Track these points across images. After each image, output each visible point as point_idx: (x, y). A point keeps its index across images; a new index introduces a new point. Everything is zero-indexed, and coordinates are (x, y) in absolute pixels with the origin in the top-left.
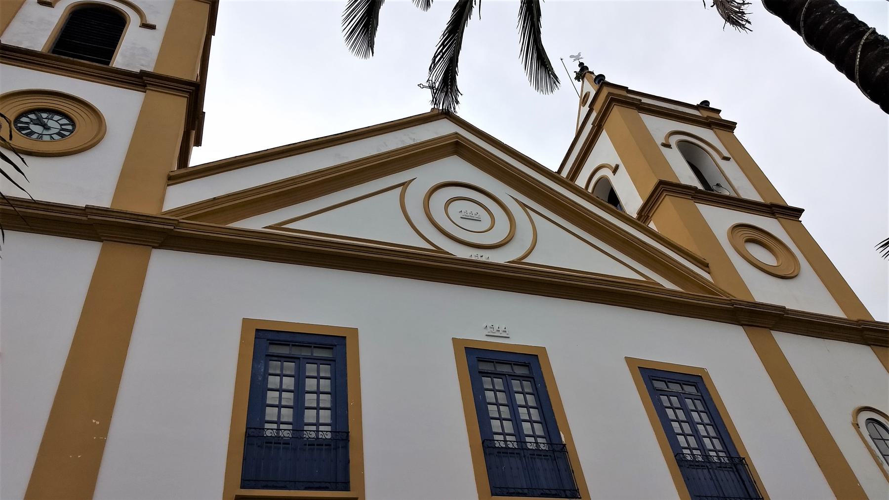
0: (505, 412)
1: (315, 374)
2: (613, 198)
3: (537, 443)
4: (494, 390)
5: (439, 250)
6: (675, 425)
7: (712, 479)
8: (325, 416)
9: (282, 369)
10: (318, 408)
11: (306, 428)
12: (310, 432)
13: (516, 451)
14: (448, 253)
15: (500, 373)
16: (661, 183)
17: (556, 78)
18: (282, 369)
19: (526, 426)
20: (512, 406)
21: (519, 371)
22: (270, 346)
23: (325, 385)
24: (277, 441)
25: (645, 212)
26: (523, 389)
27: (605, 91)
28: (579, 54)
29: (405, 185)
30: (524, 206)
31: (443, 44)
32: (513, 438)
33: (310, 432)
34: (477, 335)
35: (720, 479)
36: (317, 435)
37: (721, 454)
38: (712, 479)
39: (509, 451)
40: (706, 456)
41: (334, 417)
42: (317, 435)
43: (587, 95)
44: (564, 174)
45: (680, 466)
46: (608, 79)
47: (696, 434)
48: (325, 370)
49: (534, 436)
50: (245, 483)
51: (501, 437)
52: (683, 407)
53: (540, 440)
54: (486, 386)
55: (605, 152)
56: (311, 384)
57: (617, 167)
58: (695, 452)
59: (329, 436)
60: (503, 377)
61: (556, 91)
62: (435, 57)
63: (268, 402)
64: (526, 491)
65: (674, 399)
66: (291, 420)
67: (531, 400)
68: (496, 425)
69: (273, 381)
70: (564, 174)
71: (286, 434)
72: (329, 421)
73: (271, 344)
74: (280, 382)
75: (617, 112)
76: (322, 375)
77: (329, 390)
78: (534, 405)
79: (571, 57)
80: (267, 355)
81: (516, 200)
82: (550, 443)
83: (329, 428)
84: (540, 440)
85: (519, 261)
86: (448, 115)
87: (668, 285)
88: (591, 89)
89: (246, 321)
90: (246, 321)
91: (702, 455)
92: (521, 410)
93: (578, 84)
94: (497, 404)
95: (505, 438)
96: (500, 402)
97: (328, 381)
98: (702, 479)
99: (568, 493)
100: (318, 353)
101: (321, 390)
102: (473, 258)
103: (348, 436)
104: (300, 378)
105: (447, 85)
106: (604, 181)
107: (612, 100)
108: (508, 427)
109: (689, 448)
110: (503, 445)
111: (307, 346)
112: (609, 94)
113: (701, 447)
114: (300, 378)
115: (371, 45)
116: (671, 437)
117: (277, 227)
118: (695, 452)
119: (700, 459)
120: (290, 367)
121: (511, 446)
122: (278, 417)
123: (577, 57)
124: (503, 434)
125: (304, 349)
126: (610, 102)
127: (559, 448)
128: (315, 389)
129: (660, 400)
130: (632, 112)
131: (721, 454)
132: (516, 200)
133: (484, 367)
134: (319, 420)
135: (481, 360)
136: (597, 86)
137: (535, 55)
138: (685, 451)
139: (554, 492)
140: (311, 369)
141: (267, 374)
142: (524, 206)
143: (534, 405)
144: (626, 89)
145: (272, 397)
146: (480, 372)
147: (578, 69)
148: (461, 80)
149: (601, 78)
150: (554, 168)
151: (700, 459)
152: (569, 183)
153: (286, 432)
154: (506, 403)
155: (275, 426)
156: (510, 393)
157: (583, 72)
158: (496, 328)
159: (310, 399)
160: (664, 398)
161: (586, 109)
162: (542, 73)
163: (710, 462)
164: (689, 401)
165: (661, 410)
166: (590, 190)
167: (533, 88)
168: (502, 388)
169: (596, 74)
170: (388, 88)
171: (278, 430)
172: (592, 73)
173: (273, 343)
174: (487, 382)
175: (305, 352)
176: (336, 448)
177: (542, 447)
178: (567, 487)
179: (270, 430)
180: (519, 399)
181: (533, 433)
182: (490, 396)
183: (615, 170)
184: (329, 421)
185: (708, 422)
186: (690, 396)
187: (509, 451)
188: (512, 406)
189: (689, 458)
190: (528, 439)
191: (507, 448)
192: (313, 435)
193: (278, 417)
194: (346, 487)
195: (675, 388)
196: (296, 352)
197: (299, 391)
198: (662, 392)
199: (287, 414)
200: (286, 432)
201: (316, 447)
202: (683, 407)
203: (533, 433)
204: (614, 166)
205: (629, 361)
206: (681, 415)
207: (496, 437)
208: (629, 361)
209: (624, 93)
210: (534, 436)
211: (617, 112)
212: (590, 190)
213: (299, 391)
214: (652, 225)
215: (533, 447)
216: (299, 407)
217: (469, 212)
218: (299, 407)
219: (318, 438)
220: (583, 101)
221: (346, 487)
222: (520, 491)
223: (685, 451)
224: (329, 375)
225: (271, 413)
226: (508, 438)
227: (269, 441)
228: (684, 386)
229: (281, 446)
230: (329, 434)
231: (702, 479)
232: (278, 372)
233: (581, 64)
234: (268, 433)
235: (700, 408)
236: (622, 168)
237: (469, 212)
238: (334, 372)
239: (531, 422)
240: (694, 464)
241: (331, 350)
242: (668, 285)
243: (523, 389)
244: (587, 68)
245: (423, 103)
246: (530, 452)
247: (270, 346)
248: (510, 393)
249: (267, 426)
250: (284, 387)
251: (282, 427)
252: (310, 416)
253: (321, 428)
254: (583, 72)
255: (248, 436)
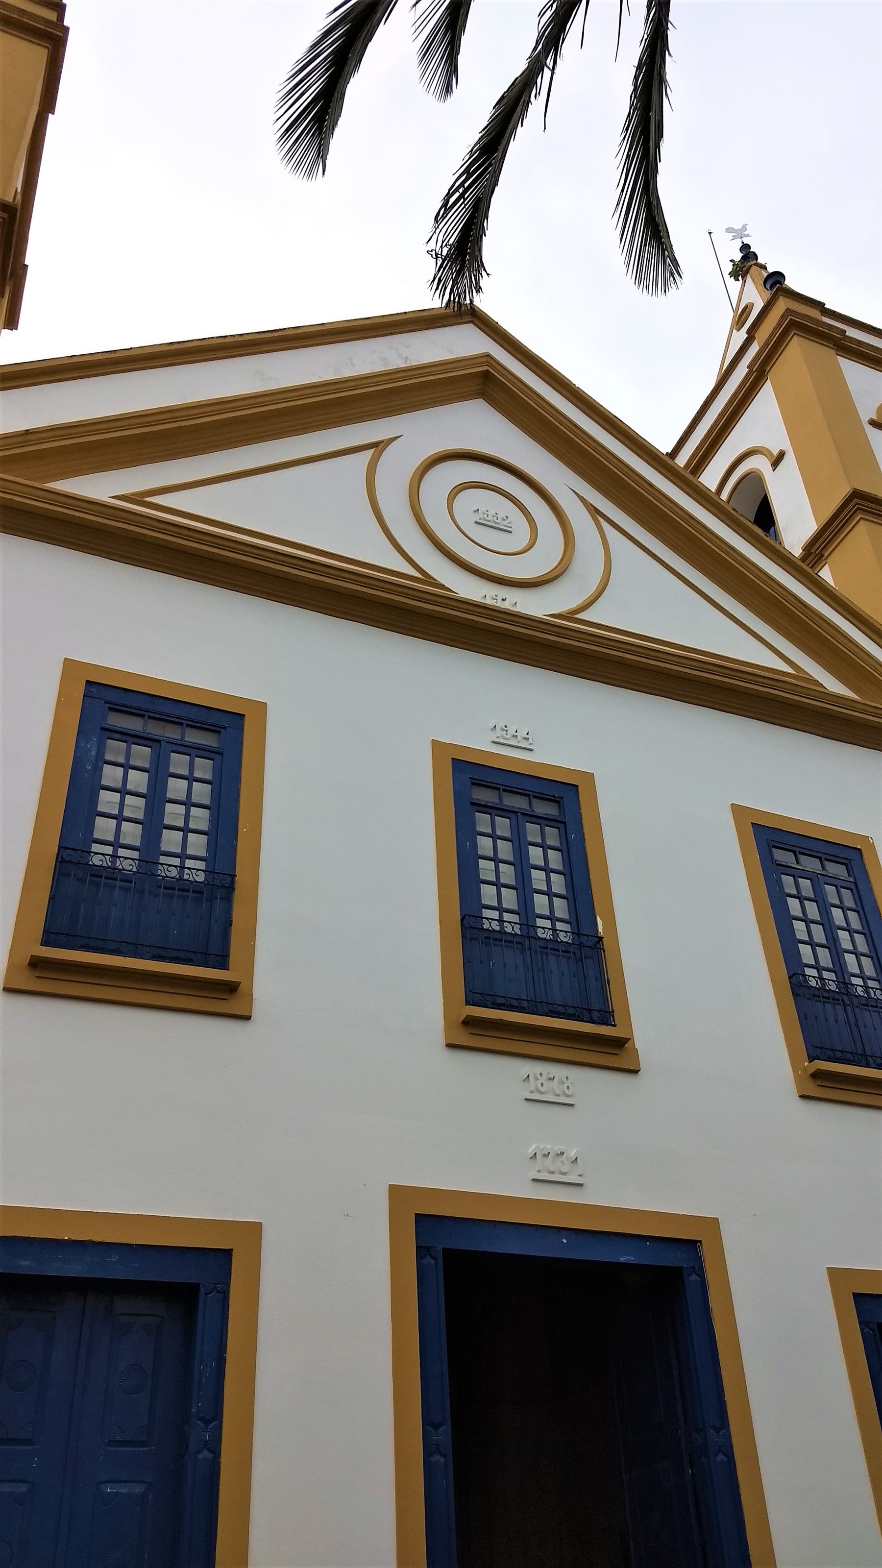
0: (508, 873)
1: (186, 772)
2: (765, 517)
3: (554, 930)
4: (494, 836)
5: (428, 579)
6: (799, 926)
7: (848, 1023)
8: (197, 844)
9: (128, 755)
10: (186, 830)
11: (163, 859)
12: (168, 867)
13: (515, 940)
14: (442, 587)
15: (508, 808)
16: (856, 495)
17: (676, 264)
18: (128, 755)
19: (540, 902)
20: (522, 866)
21: (542, 808)
22: (111, 713)
23: (202, 792)
24: (110, 875)
25: (819, 547)
26: (543, 839)
27: (782, 305)
28: (744, 227)
29: (378, 447)
30: (595, 512)
31: (467, 171)
32: (515, 918)
33: (168, 867)
34: (477, 740)
35: (861, 1025)
36: (181, 873)
37: (871, 984)
38: (848, 1023)
39: (505, 938)
40: (844, 983)
41: (212, 846)
42: (181, 873)
43: (748, 309)
44: (681, 461)
45: (795, 994)
46: (791, 282)
47: (833, 945)
48: (204, 768)
49: (552, 918)
50: (49, 938)
51: (495, 915)
52: (819, 899)
53: (559, 926)
54: (480, 828)
55: (764, 423)
56: (176, 788)
57: (781, 455)
58: (826, 975)
59: (201, 877)
60: (511, 815)
61: (672, 291)
62: (449, 195)
63: (101, 808)
64: (525, 1004)
65: (805, 884)
66: (137, 843)
67: (555, 859)
68: (488, 893)
69: (111, 775)
70: (681, 461)
71: (126, 865)
72: (203, 853)
73: (111, 709)
74: (123, 779)
75: (797, 349)
76: (197, 774)
77: (207, 802)
78: (560, 867)
79: (729, 230)
80: (103, 729)
81: (582, 499)
82: (577, 933)
83: (201, 865)
84: (559, 926)
85: (570, 616)
86: (462, 313)
87: (833, 685)
88: (756, 298)
89: (69, 665)
90: (69, 665)
91: (837, 982)
92: (535, 873)
93: (735, 286)
94: (496, 860)
95: (501, 916)
96: (501, 856)
97: (208, 787)
98: (832, 1020)
99: (595, 1015)
100: (194, 737)
101: (194, 799)
102: (488, 601)
103: (233, 882)
104: (158, 775)
105: (463, 256)
106: (754, 480)
107: (793, 325)
108: (510, 898)
109: (862, 976)
110: (496, 926)
111: (176, 721)
112: (788, 311)
113: (839, 967)
114: (158, 775)
115: (322, 153)
116: (788, 944)
117: (137, 498)
118: (826, 975)
119: (833, 987)
120: (142, 754)
121: (509, 929)
122: (115, 835)
123: (739, 233)
124: (500, 909)
125: (170, 727)
126: (787, 326)
127: (591, 942)
128: (183, 797)
129: (780, 883)
130: (825, 353)
131: (871, 984)
132: (582, 499)
133: (784, 857)
134: (185, 848)
135: (476, 783)
136: (768, 295)
137: (643, 215)
138: (855, 981)
139: (571, 1011)
140: (178, 762)
141: (101, 761)
142: (595, 512)
143: (560, 867)
144: (819, 305)
145: (108, 801)
146: (472, 804)
147: (738, 256)
148: (491, 247)
149: (775, 280)
150: (665, 446)
151: (833, 987)
152: (687, 480)
153: (128, 860)
154: (511, 859)
155: (109, 850)
156: (519, 843)
157: (746, 263)
158: (511, 731)
159: (173, 813)
160: (787, 880)
161: (741, 336)
162: (650, 252)
163: (848, 994)
164: (830, 890)
165: (777, 900)
166: (724, 496)
167: (630, 279)
168: (557, 844)
169: (771, 270)
170: (349, 248)
171: (115, 856)
172: (764, 267)
173: (116, 708)
174: (483, 821)
175: (172, 733)
176: (212, 899)
177: (562, 937)
178: (595, 1005)
179: (99, 856)
180: (535, 855)
181: (551, 912)
182: (485, 845)
183: (777, 461)
184: (203, 853)
185: (860, 928)
186: (833, 881)
187: (505, 938)
188: (522, 866)
189: (813, 983)
190: (540, 922)
191: (502, 932)
192: (174, 873)
193: (115, 835)
194: (223, 963)
195: (811, 864)
196: (155, 729)
197: (156, 798)
198: (786, 869)
199: (132, 833)
200: (128, 860)
201: (177, 892)
202: (819, 899)
203: (551, 912)
204: (775, 453)
205: (738, 811)
206: (813, 911)
207: (487, 913)
208: (738, 811)
209: (815, 314)
210: (552, 918)
211: (797, 349)
212: (724, 496)
213: (156, 798)
214: (826, 574)
215: (548, 935)
216: (153, 824)
217: (491, 513)
218: (153, 824)
219: (181, 879)
220: (739, 321)
221: (223, 963)
222: (515, 1003)
223: (809, 971)
224: (208, 776)
225: (104, 828)
226: (507, 916)
227: (97, 873)
228: (801, 857)
229: (118, 883)
230: (202, 874)
231: (832, 1020)
232: (121, 760)
233: (745, 247)
234: (96, 860)
235: (849, 902)
236: (790, 460)
237: (491, 513)
238: (218, 771)
239: (550, 894)
240: (821, 994)
241: (215, 736)
242: (833, 685)
243: (543, 839)
244: (756, 257)
245: (415, 288)
246: (542, 944)
247: (111, 713)
248: (519, 843)
249: (95, 848)
250: (130, 787)
251: (122, 852)
252: (171, 840)
253: (189, 863)
254: (746, 263)
255: (61, 861)
